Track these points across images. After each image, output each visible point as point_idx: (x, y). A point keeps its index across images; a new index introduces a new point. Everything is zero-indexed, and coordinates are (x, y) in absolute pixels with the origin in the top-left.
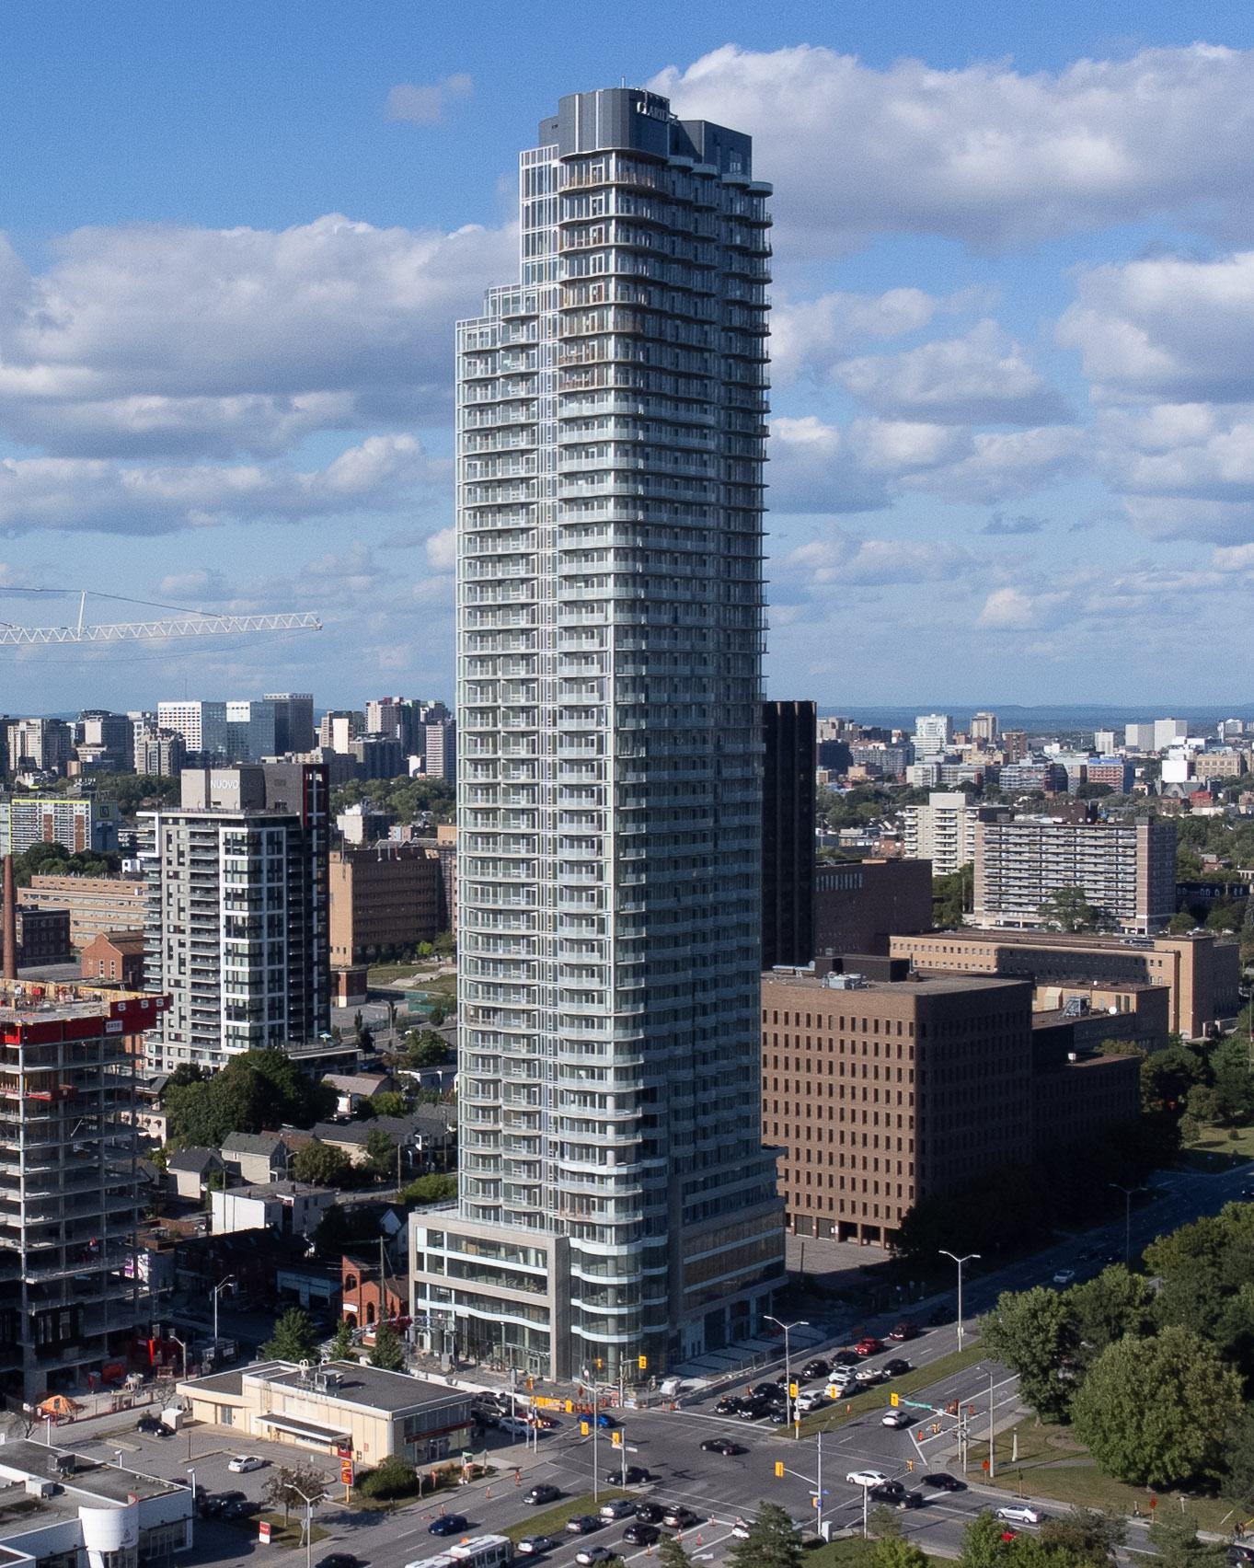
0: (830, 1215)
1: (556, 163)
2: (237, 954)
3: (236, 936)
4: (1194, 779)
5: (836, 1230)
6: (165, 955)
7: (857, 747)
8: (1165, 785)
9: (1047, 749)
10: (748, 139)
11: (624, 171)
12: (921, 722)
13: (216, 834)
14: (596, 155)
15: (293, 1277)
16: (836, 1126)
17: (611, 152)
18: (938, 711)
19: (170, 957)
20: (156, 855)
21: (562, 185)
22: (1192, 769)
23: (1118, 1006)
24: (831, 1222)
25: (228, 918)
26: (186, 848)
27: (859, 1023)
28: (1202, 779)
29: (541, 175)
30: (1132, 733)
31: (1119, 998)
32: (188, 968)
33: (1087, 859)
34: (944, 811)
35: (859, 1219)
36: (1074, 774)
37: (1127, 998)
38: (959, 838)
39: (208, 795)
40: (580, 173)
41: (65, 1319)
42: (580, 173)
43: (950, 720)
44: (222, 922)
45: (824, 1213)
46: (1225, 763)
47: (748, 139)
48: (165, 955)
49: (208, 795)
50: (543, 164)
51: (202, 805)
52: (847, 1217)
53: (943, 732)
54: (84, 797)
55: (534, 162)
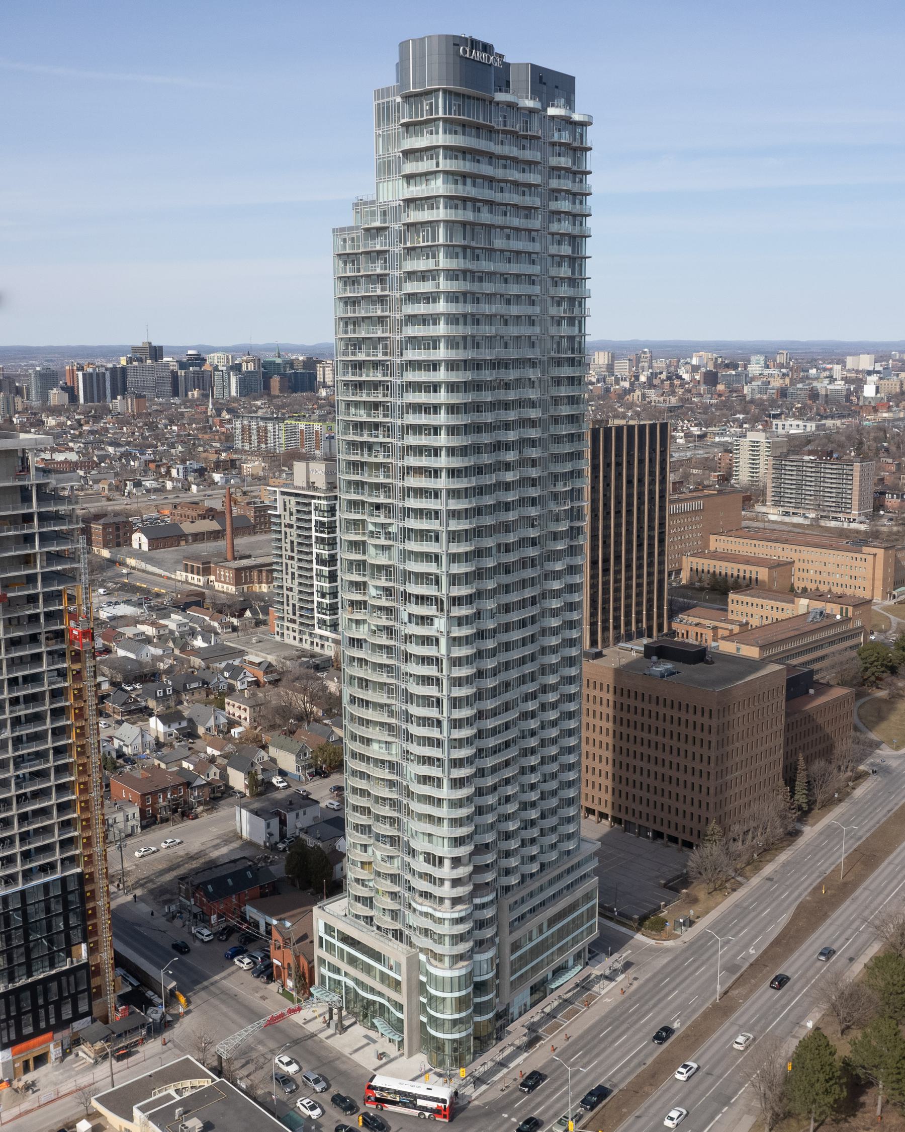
0: (647, 824)
1: (399, 99)
2: (322, 576)
3: (322, 565)
4: (879, 395)
5: (650, 834)
6: (284, 572)
7: (723, 372)
8: (865, 398)
9: (810, 371)
10: (572, 79)
11: (447, 109)
12: (753, 358)
13: (310, 504)
14: (428, 93)
15: (255, 911)
16: (669, 712)
17: (437, 90)
18: (761, 353)
19: (287, 574)
20: (278, 513)
21: (403, 118)
22: (877, 392)
23: (841, 615)
24: (647, 829)
25: (318, 555)
26: (294, 510)
27: (668, 702)
28: (883, 395)
29: (388, 108)
30: (850, 362)
31: (842, 608)
32: (296, 581)
33: (827, 480)
34: (754, 442)
35: (664, 829)
36: (823, 392)
37: (847, 609)
38: (761, 448)
39: (308, 478)
40: (417, 108)
41: (54, 986)
42: (417, 108)
43: (766, 357)
44: (314, 556)
45: (643, 822)
46: (893, 385)
47: (572, 79)
48: (284, 572)
49: (308, 478)
50: (390, 99)
51: (305, 485)
52: (658, 828)
53: (762, 363)
54: (319, 421)
55: (383, 98)
